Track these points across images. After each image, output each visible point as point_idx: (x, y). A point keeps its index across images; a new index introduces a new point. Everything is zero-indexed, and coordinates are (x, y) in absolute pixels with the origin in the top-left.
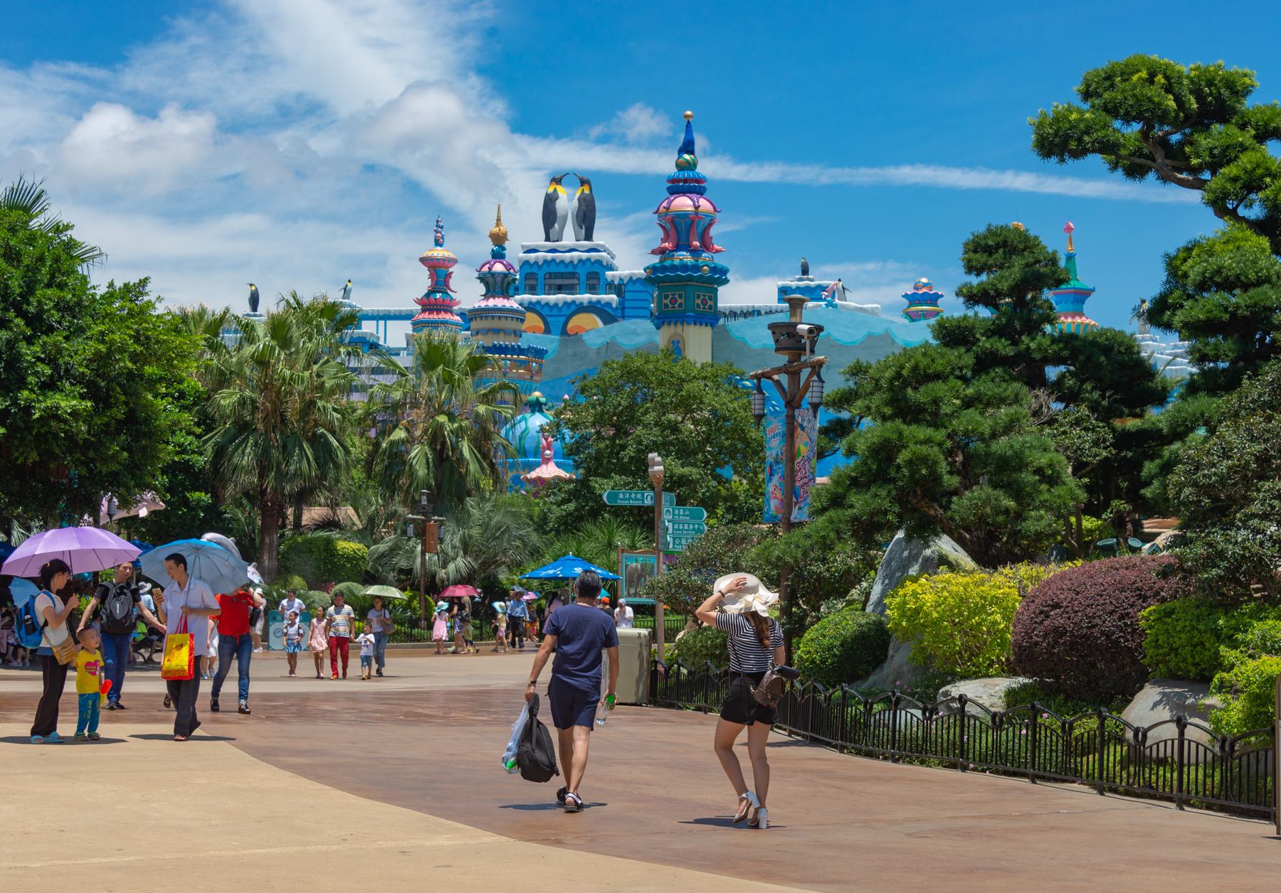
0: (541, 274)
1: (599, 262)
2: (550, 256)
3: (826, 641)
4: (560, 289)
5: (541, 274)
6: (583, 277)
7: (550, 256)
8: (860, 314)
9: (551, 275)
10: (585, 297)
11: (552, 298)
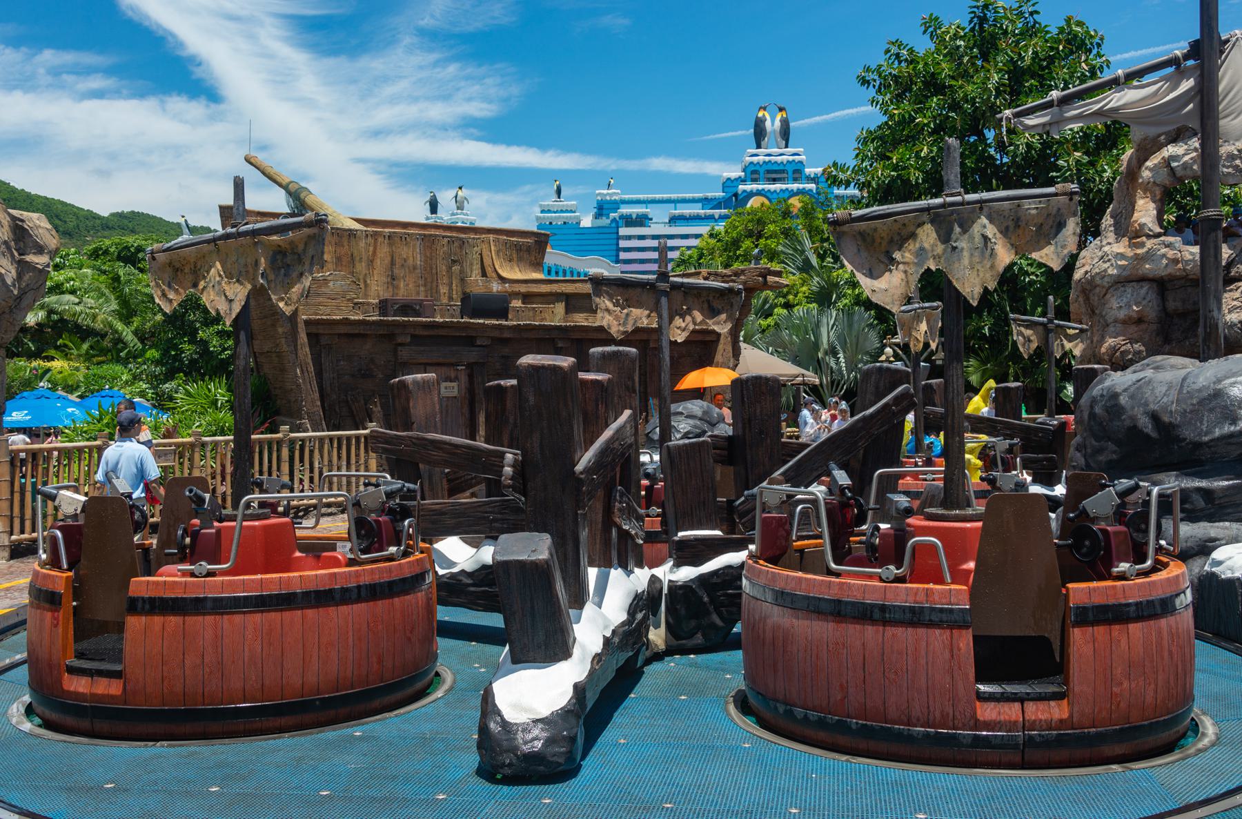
0: (762, 171)
1: (801, 162)
2: (767, 159)
3: (1097, 242)
4: (774, 180)
5: (762, 171)
6: (790, 173)
7: (767, 159)
8: (326, 375)
9: (768, 172)
10: (795, 186)
11: (772, 187)
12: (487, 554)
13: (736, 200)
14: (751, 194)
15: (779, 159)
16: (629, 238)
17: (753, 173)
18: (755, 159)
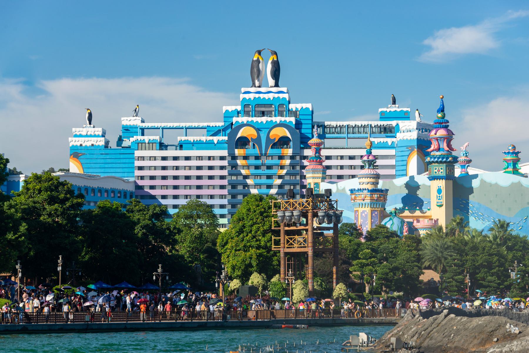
4: (263, 114)
9: (258, 105)
10: (278, 119)
11: (260, 119)
12: (366, 285)
13: (231, 128)
14: (243, 125)
15: (266, 96)
16: (143, 158)
17: (247, 109)
18: (247, 96)
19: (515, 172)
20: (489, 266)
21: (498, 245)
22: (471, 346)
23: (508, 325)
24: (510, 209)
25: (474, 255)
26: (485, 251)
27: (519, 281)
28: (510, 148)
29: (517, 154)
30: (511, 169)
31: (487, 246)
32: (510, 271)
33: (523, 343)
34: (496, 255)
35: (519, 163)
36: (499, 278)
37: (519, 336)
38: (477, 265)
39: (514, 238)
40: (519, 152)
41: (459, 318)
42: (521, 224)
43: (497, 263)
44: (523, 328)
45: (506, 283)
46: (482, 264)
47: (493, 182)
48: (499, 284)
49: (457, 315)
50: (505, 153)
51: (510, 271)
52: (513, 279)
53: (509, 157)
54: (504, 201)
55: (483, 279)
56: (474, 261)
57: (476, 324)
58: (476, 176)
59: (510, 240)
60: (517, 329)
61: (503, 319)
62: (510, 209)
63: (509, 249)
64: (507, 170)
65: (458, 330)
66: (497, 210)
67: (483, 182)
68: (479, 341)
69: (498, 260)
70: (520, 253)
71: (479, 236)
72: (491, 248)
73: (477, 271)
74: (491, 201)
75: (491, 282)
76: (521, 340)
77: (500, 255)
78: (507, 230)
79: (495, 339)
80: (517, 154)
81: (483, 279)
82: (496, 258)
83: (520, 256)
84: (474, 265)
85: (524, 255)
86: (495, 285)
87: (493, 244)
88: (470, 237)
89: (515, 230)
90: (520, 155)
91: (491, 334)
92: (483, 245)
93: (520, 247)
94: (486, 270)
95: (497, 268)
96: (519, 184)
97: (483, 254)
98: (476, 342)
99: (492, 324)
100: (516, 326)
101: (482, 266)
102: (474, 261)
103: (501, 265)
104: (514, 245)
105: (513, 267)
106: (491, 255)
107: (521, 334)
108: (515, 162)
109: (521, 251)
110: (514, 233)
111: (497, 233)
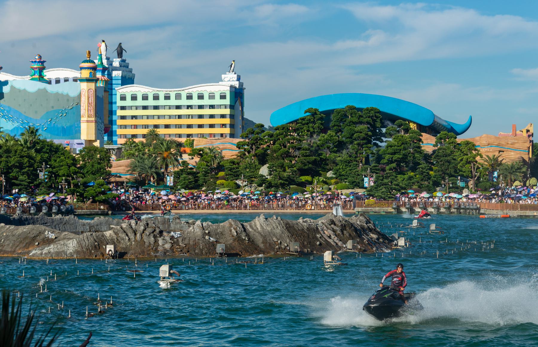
19: (41, 79)
20: (20, 166)
21: (29, 148)
22: (18, 248)
23: (47, 232)
24: (36, 112)
25: (7, 157)
26: (17, 154)
27: (46, 180)
28: (37, 57)
29: (42, 63)
30: (37, 76)
31: (19, 149)
32: (38, 171)
33: (59, 247)
34: (26, 157)
35: (44, 71)
36: (29, 176)
37: (55, 240)
38: (10, 165)
39: (42, 142)
40: (44, 62)
41: (8, 226)
42: (46, 125)
43: (27, 164)
44: (58, 234)
45: (35, 182)
46: (14, 164)
47: (22, 88)
48: (29, 183)
49: (6, 224)
50: (32, 62)
51: (38, 171)
52: (41, 179)
53: (35, 66)
54: (31, 105)
55: (16, 178)
56: (8, 162)
57: (21, 231)
58: (6, 83)
59: (38, 143)
60: (53, 235)
61: (43, 227)
62: (36, 112)
63: (38, 151)
64: (33, 77)
65: (7, 236)
66: (25, 113)
67: (12, 87)
68: (24, 245)
69: (28, 161)
70: (47, 155)
71: (12, 140)
72: (22, 150)
73: (10, 171)
74: (20, 105)
75: (22, 181)
76: (56, 244)
77: (30, 157)
78: (36, 135)
79: (37, 243)
80: (42, 63)
81: (16, 178)
82: (26, 160)
83: (47, 158)
84: (8, 165)
85: (50, 157)
86: (26, 183)
87: (24, 148)
88: (4, 141)
89: (43, 135)
90: (45, 64)
91: (34, 239)
92: (16, 148)
93: (47, 149)
94: (17, 170)
95: (27, 169)
96: (45, 91)
97: (15, 155)
98: (21, 246)
99: (34, 232)
100: (52, 233)
101: (14, 166)
102: (8, 162)
103: (31, 165)
104: (42, 148)
105: (41, 167)
106: (22, 157)
107: (57, 239)
108: (41, 70)
109: (48, 153)
110: (41, 138)
111: (27, 138)
